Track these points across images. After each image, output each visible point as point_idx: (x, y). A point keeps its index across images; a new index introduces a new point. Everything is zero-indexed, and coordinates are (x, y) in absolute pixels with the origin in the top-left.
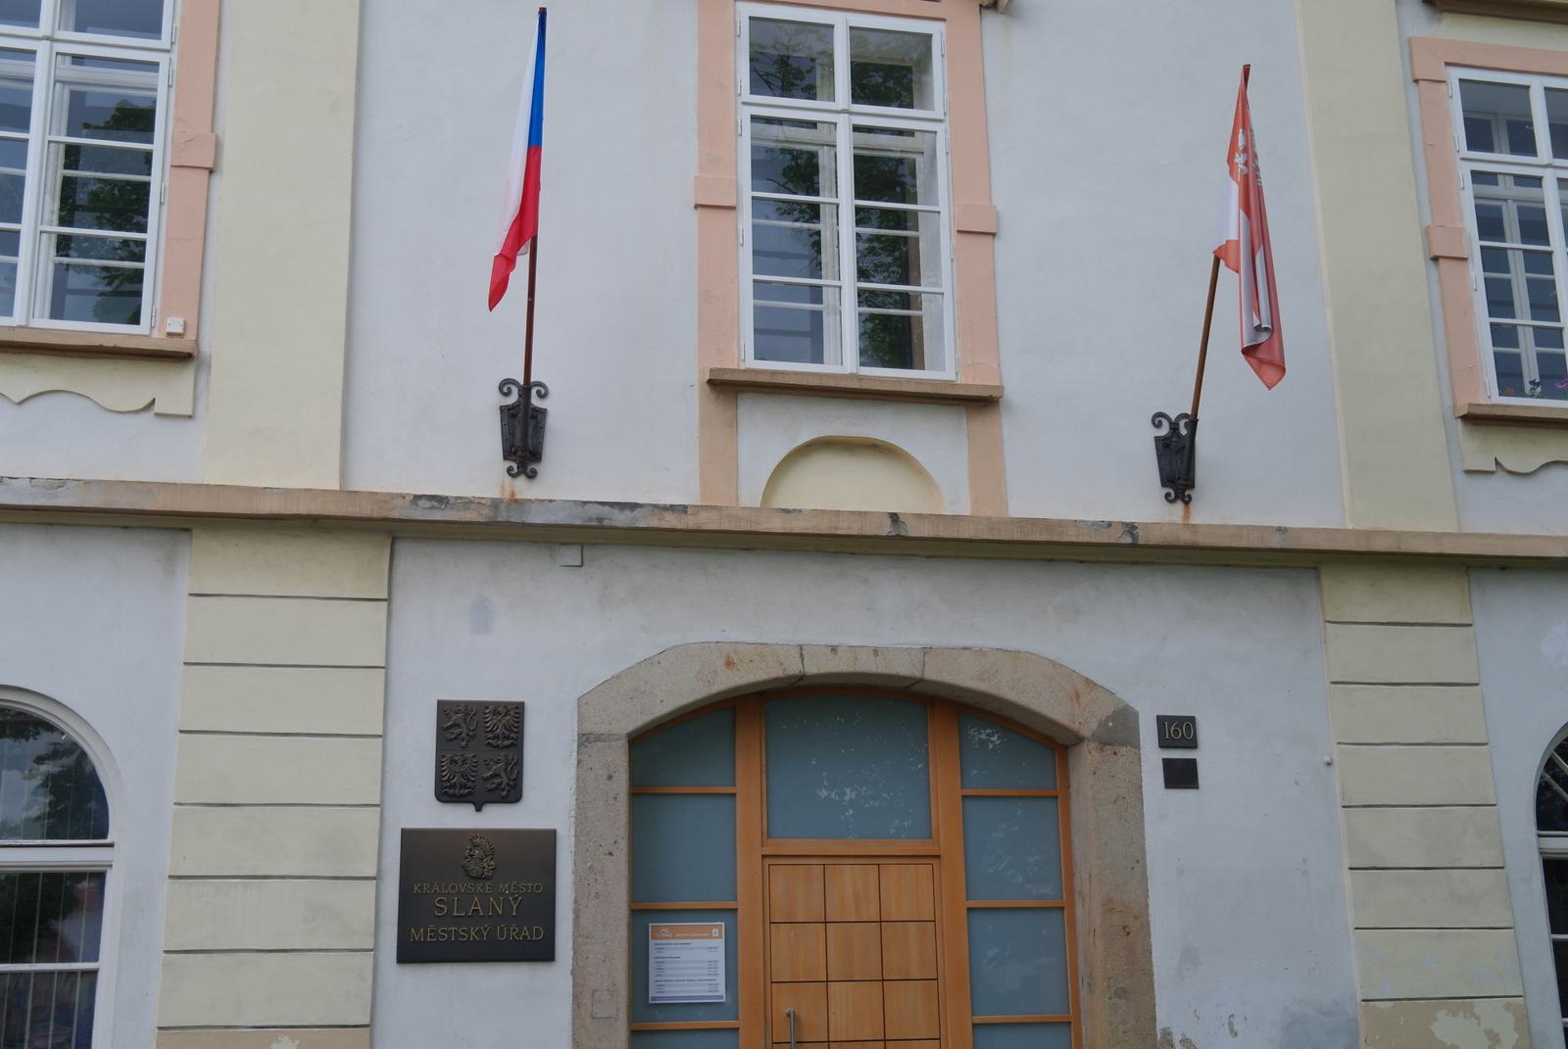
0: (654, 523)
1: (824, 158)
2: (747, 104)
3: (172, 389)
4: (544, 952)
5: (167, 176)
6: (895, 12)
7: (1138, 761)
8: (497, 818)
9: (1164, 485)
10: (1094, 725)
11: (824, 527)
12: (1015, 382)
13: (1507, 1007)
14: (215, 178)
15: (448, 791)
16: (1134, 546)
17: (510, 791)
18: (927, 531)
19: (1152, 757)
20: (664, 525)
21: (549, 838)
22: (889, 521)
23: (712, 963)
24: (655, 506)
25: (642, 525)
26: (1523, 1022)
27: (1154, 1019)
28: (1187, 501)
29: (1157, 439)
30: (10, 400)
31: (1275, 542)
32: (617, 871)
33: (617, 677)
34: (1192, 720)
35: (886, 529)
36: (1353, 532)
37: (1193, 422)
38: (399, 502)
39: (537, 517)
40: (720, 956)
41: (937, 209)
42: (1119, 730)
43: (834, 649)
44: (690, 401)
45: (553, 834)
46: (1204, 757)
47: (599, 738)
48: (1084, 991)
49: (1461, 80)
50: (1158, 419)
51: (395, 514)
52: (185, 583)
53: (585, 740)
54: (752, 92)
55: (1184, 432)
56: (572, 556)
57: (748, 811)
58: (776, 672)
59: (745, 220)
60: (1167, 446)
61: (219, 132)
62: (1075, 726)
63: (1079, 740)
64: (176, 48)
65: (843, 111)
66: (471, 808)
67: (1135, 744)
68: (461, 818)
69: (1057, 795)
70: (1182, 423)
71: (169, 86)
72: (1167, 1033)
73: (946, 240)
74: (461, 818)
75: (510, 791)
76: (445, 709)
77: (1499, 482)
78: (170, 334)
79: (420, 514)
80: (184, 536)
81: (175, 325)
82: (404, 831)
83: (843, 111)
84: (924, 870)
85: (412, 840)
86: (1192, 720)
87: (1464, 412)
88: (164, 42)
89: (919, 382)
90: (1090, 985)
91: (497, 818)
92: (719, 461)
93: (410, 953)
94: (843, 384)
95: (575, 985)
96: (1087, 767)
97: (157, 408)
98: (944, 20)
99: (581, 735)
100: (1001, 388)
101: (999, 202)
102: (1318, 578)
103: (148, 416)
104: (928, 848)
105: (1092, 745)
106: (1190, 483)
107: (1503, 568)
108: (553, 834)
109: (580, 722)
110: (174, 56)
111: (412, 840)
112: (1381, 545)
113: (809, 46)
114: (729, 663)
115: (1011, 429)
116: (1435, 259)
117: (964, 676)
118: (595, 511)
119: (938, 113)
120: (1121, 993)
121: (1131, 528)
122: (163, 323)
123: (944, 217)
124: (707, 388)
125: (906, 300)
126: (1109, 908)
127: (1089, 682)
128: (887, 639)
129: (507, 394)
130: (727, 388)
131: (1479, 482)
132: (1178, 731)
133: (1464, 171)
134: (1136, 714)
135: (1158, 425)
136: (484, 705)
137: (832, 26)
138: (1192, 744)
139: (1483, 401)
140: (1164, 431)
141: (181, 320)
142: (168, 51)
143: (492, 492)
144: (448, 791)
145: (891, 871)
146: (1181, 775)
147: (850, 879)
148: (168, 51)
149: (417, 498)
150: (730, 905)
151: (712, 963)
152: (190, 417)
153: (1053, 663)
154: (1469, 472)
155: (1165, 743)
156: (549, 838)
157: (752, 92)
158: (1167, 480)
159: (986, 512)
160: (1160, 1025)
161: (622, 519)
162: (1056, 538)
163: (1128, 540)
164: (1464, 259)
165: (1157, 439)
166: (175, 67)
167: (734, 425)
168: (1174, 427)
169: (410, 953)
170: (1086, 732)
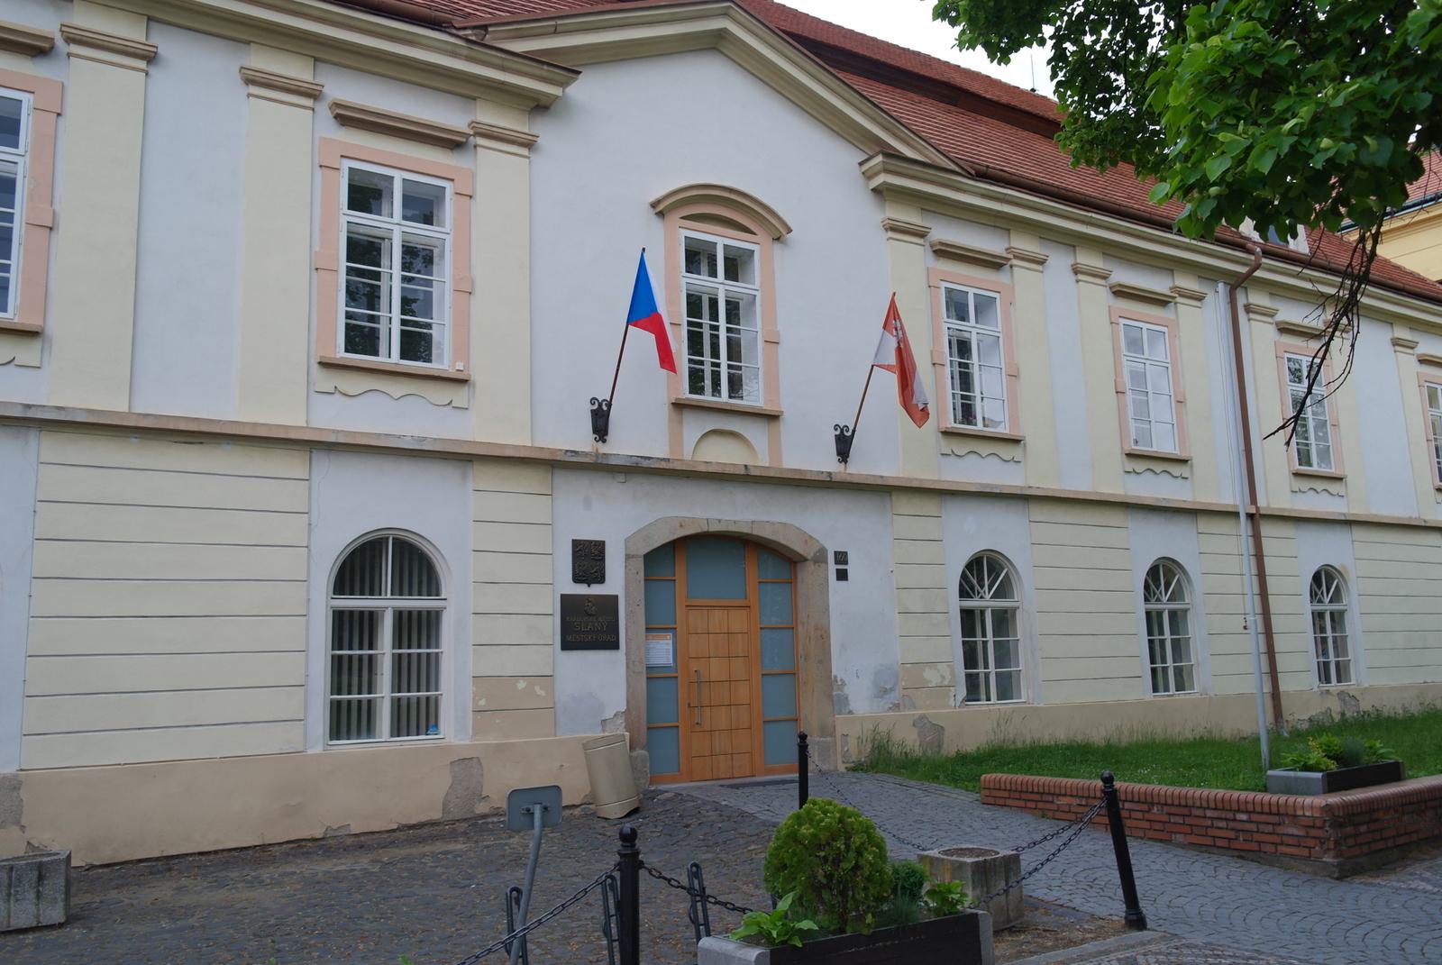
0: (657, 466)
1: (385, 246)
2: (346, 217)
3: (459, 396)
4: (614, 646)
5: (23, 229)
6: (367, 159)
7: (827, 569)
8: (596, 590)
9: (838, 455)
10: (812, 555)
11: (719, 470)
12: (785, 405)
13: (948, 666)
14: (54, 234)
15: (577, 579)
16: (831, 481)
17: (600, 579)
18: (757, 473)
19: (832, 568)
20: (661, 467)
21: (615, 599)
22: (743, 468)
23: (667, 650)
24: (658, 458)
25: (653, 466)
26: (952, 672)
27: (831, 672)
28: (846, 462)
29: (836, 436)
30: (392, 397)
31: (879, 482)
32: (641, 612)
33: (639, 531)
34: (846, 553)
35: (743, 472)
36: (903, 478)
37: (609, 405)
38: (560, 453)
39: (613, 462)
40: (671, 647)
41: (443, 280)
42: (820, 557)
43: (720, 521)
44: (665, 411)
45: (617, 596)
46: (851, 568)
47: (633, 556)
48: (802, 661)
49: (350, 168)
50: (593, 400)
51: (558, 458)
52: (471, 485)
53: (628, 557)
54: (349, 209)
55: (605, 408)
56: (621, 478)
57: (680, 588)
58: (699, 531)
59: (948, 370)
60: (839, 439)
61: (57, 207)
62: (805, 555)
63: (805, 560)
64: (28, 154)
65: (397, 224)
66: (586, 585)
67: (826, 562)
68: (582, 589)
69: (792, 582)
70: (604, 403)
71: (24, 177)
72: (836, 677)
73: (448, 297)
74: (582, 589)
75: (600, 579)
76: (576, 543)
77: (952, 458)
78: (458, 370)
79: (568, 458)
80: (470, 464)
81: (460, 366)
82: (562, 595)
83: (397, 224)
84: (744, 612)
85: (565, 599)
86: (846, 553)
87: (943, 430)
88: (21, 151)
89: (703, 401)
90: (805, 659)
91: (596, 590)
92: (676, 439)
93: (567, 645)
94: (1153, 455)
95: (627, 659)
96: (807, 575)
97: (16, 362)
98: (33, 93)
99: (626, 555)
100: (43, 329)
101: (779, 328)
102: (890, 496)
103: (450, 407)
104: (745, 603)
105: (812, 563)
106: (606, 433)
107: (953, 494)
108: (617, 596)
109: (626, 550)
110: (27, 159)
111: (565, 599)
112: (915, 484)
113: (382, 185)
114: (681, 526)
115: (785, 427)
116: (934, 364)
117: (766, 533)
118: (634, 460)
119: (1000, 329)
120: (820, 662)
121: (830, 474)
122: (454, 366)
123: (760, 335)
124: (671, 406)
125: (373, 319)
126: (816, 628)
127: (811, 537)
128: (738, 517)
129: (593, 404)
130: (679, 406)
131: (945, 458)
132: (841, 558)
133: (343, 220)
134: (827, 551)
135: (836, 430)
136: (591, 542)
137: (21, 101)
138: (846, 563)
139: (949, 426)
140: (596, 407)
141: (462, 364)
142: (23, 156)
143: (588, 449)
144: (577, 579)
145: (732, 612)
146: (842, 575)
147: (718, 615)
148: (23, 156)
149: (567, 451)
150: (674, 626)
151: (667, 650)
152: (39, 368)
153: (798, 528)
154: (943, 454)
155: (837, 562)
156: (615, 599)
157: (349, 209)
158: (595, 431)
159: (775, 465)
160: (833, 674)
161: (645, 464)
162: (803, 478)
163: (829, 479)
164: (944, 365)
165: (836, 436)
166: (27, 166)
167: (681, 422)
168: (600, 405)
169: (567, 645)
170: (809, 557)
